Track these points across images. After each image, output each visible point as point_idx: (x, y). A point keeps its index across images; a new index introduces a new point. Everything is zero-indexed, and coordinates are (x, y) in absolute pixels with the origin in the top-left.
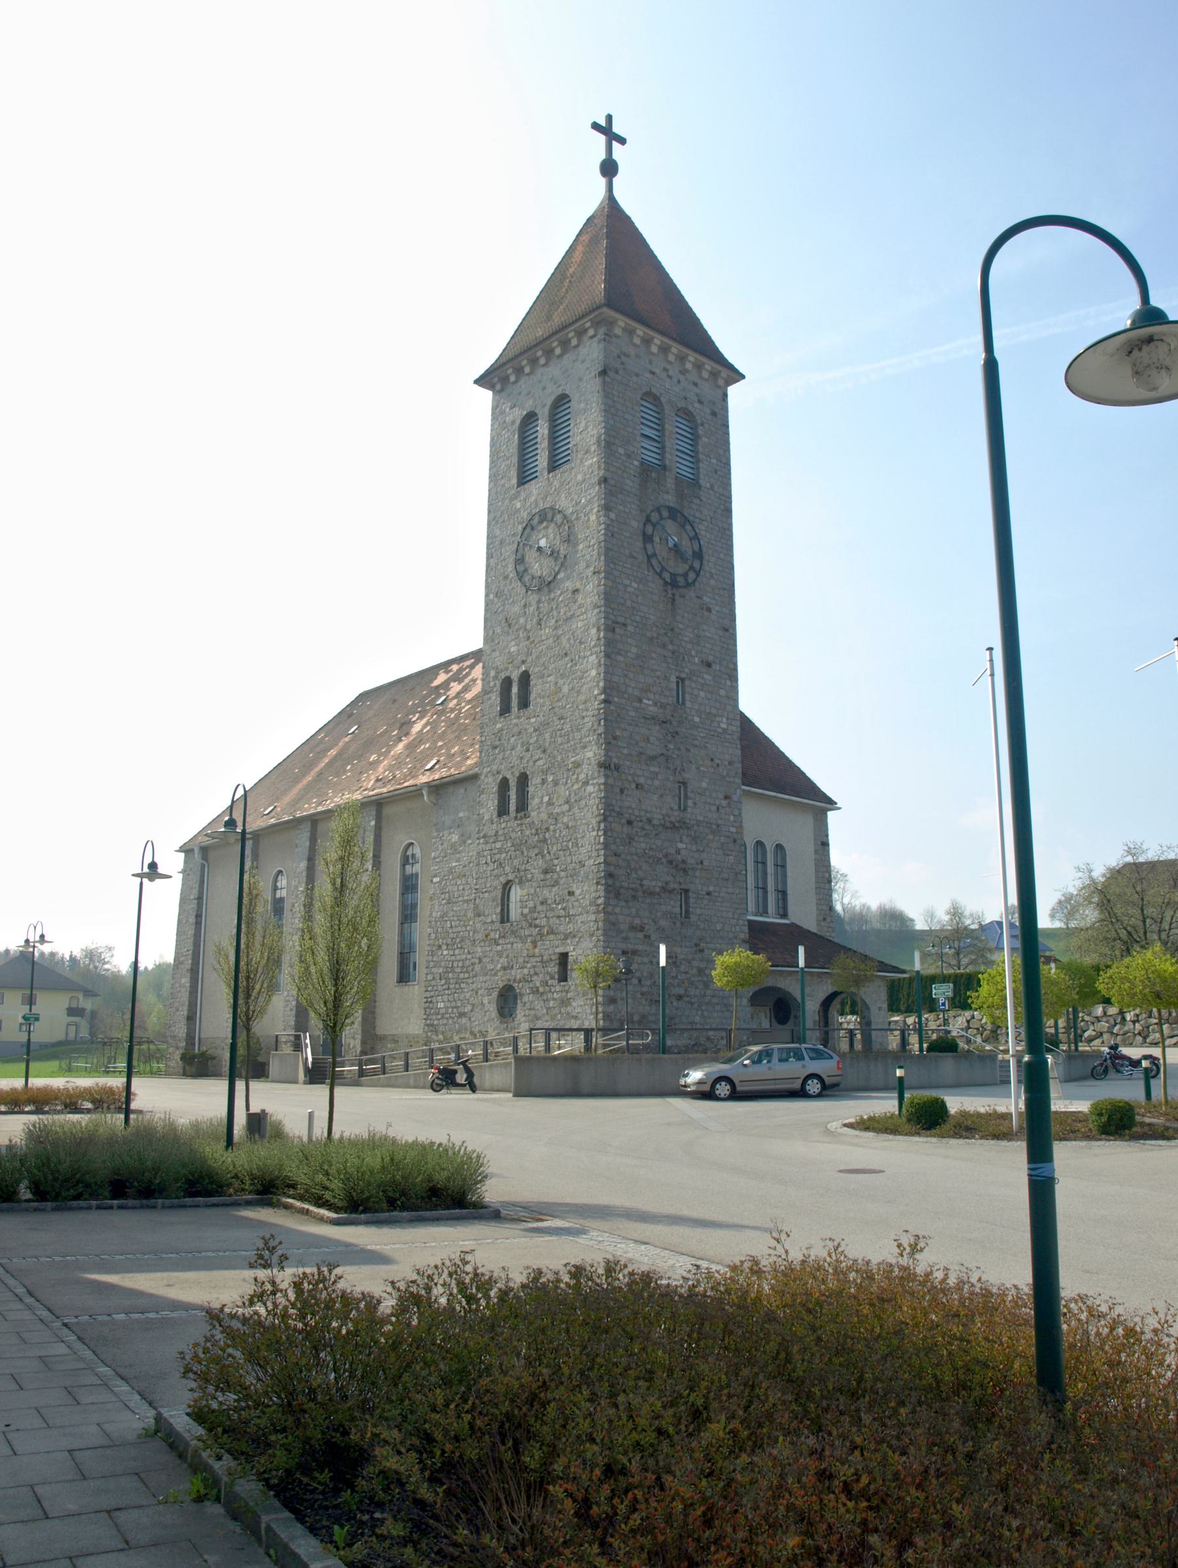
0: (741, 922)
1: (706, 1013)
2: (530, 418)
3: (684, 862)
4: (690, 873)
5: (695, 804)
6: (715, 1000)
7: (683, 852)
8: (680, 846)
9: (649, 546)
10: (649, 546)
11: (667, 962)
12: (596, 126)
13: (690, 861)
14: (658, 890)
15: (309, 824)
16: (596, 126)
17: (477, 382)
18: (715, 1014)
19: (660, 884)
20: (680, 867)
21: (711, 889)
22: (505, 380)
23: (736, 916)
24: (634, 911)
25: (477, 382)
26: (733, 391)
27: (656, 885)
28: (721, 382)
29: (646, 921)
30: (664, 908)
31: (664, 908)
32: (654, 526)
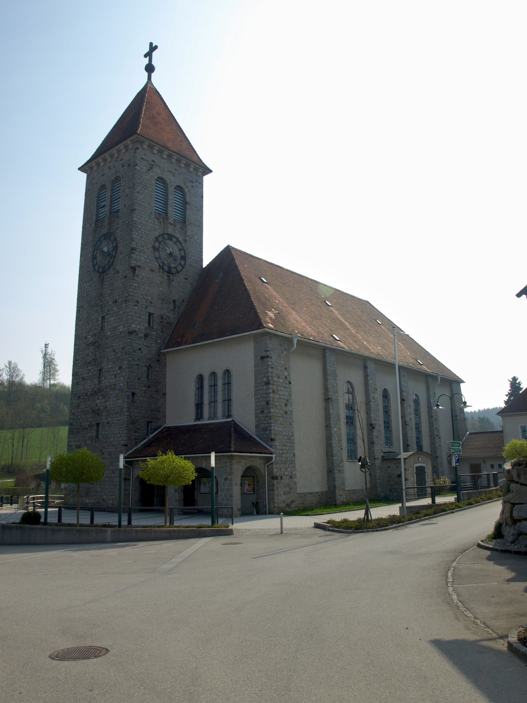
0: (123, 435)
1: (103, 486)
2: (103, 187)
3: (99, 409)
4: (101, 414)
5: (105, 378)
6: (107, 479)
7: (99, 405)
8: (98, 401)
9: (183, 254)
10: (183, 254)
11: (216, 464)
12: (151, 44)
13: (102, 408)
14: (87, 426)
15: (501, 430)
16: (151, 44)
17: (79, 169)
18: (107, 487)
19: (88, 423)
20: (97, 412)
21: (110, 420)
22: (91, 168)
23: (121, 432)
24: (78, 438)
25: (79, 169)
26: (206, 179)
27: (86, 424)
28: (200, 174)
29: (82, 442)
30: (89, 435)
31: (89, 435)
32: (160, 243)
